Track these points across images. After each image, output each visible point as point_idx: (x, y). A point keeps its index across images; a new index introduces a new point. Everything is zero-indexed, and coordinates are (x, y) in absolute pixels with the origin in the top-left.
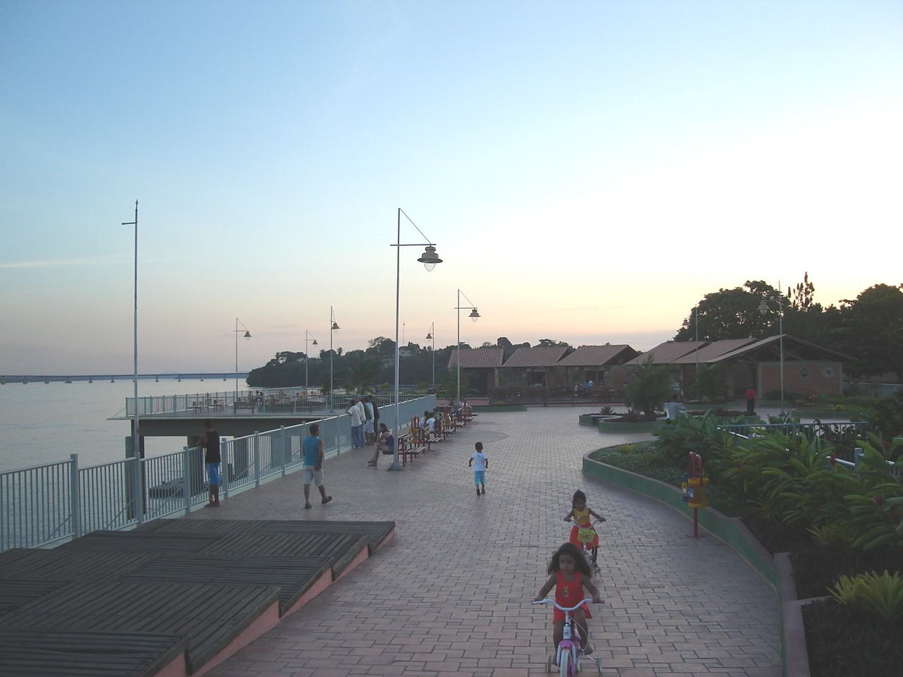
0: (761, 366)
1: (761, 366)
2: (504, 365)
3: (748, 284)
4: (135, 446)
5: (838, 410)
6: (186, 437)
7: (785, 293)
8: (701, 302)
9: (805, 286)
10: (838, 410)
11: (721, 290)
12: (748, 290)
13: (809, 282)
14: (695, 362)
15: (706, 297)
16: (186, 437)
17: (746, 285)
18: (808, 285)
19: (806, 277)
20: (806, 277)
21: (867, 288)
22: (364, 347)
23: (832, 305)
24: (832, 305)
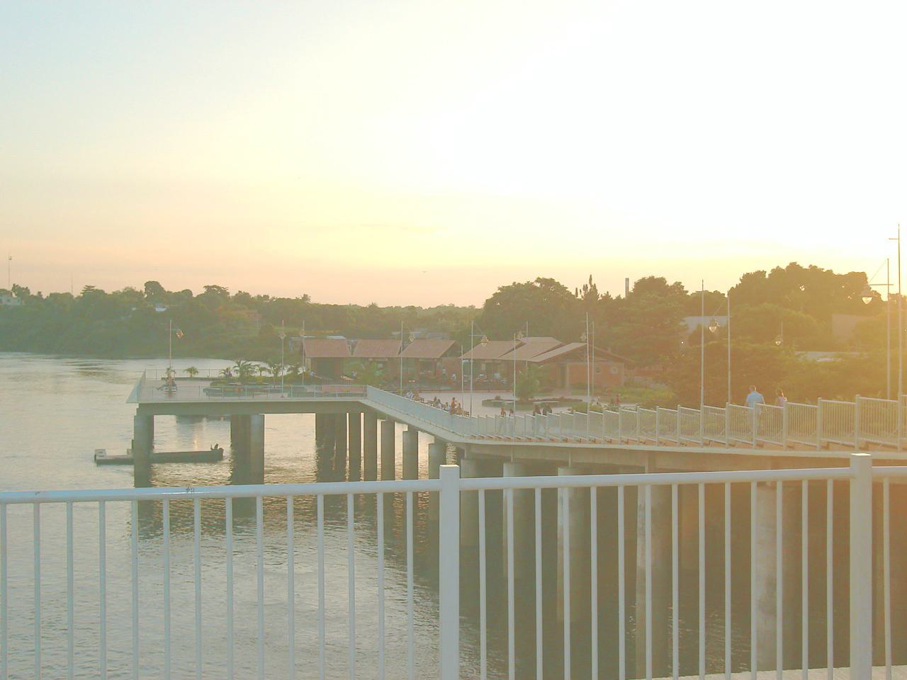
3: (538, 280)
5: (625, 398)
7: (574, 293)
8: (495, 295)
9: (589, 288)
10: (625, 398)
11: (305, 297)
12: (538, 285)
13: (593, 284)
14: (529, 338)
15: (499, 289)
17: (536, 281)
18: (591, 286)
19: (591, 279)
20: (591, 279)
22: (109, 291)
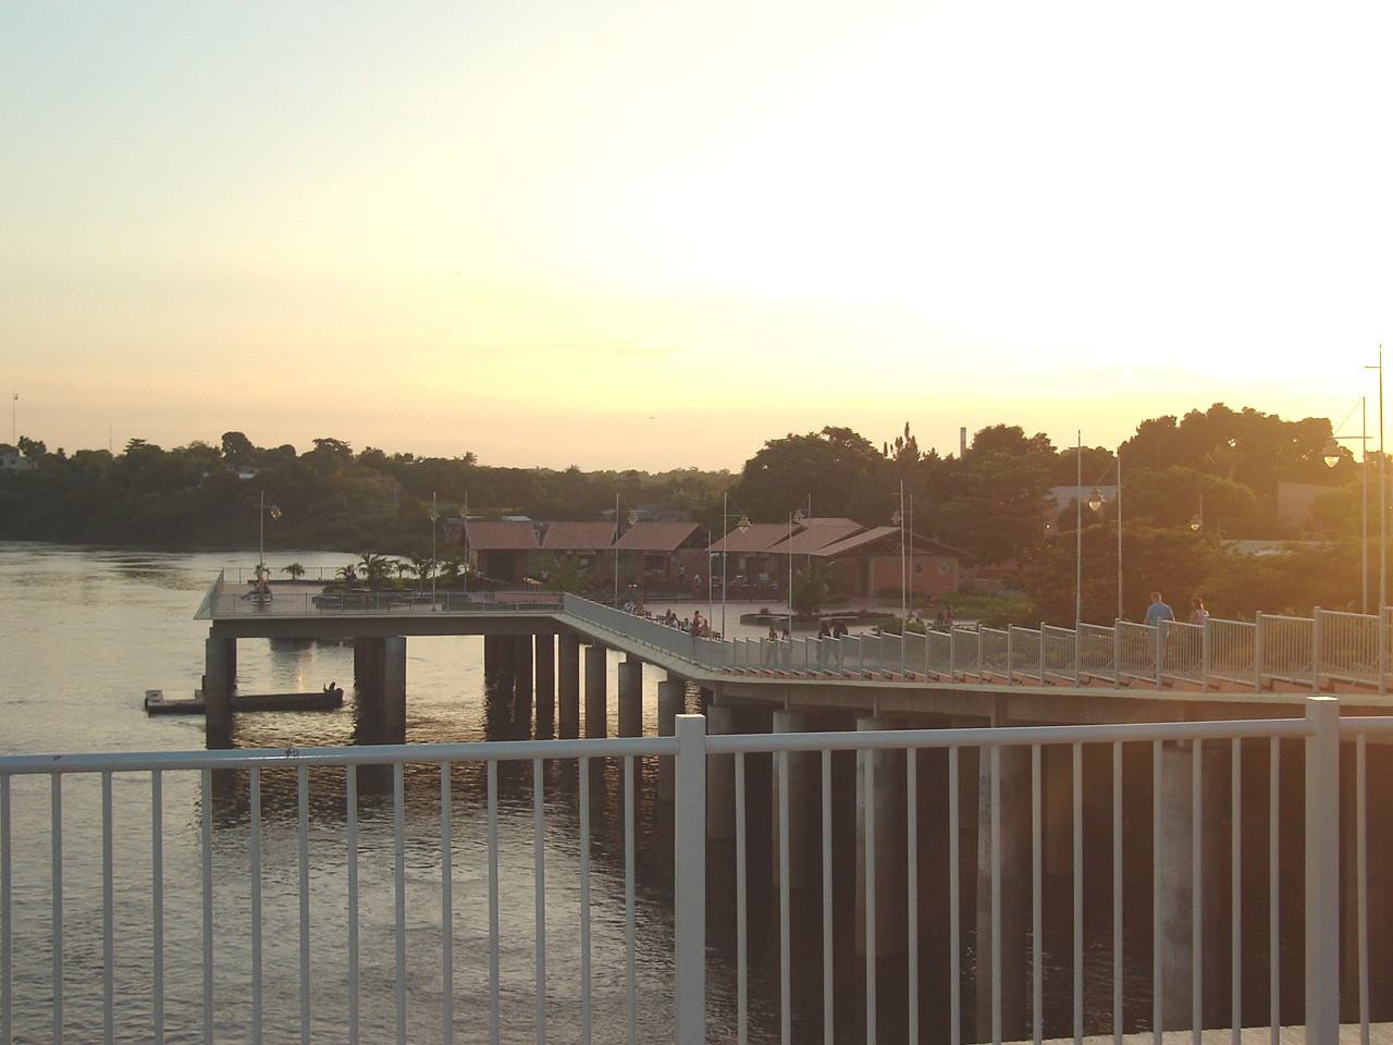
0: (874, 561)
1: (874, 561)
2: (617, 546)
3: (827, 430)
4: (561, 601)
6: (238, 640)
8: (761, 453)
9: (905, 442)
10: (960, 612)
11: (790, 435)
12: (826, 438)
13: (911, 436)
16: (238, 640)
17: (824, 432)
18: (908, 440)
19: (907, 429)
20: (907, 429)
21: (984, 427)
23: (933, 449)
24: (933, 449)
